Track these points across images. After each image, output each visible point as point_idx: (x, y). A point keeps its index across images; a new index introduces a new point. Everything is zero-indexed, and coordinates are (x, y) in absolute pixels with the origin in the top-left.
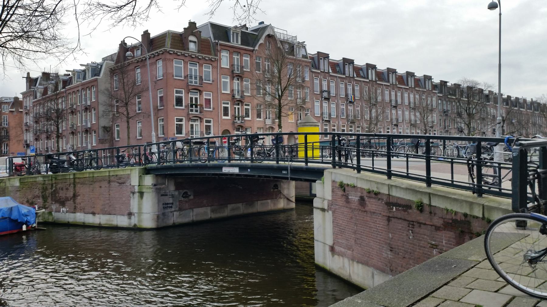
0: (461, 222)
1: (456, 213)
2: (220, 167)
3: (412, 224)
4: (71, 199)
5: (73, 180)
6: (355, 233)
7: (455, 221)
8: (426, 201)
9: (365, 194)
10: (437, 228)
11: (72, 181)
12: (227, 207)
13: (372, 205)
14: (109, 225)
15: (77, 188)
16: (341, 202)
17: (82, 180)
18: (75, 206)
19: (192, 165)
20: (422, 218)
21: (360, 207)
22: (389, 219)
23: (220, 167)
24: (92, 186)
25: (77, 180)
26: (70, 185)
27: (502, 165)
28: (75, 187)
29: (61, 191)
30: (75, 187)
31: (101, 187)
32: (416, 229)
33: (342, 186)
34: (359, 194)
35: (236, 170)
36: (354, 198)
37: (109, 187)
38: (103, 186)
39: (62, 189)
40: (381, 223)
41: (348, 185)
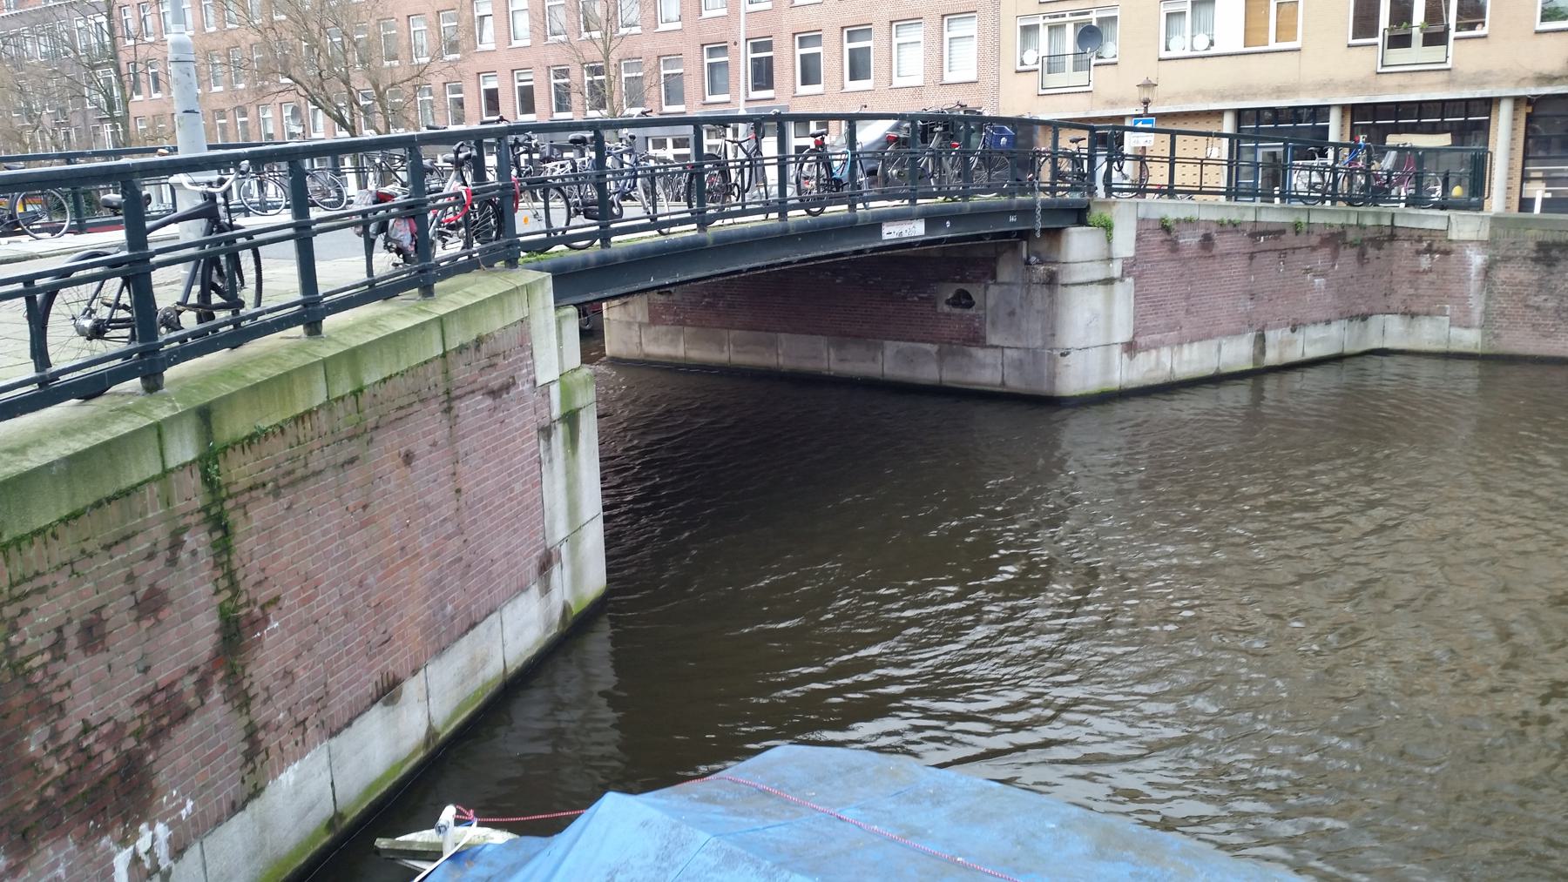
0: (1339, 234)
1: (1331, 226)
2: (875, 225)
3: (1283, 253)
4: (203, 686)
5: (194, 481)
6: (1188, 298)
7: (1333, 235)
8: (1304, 219)
9: (1214, 228)
10: (1314, 249)
11: (191, 494)
12: (881, 348)
13: (1223, 244)
14: (482, 689)
15: (246, 544)
16: (1160, 253)
17: (279, 449)
18: (251, 734)
19: (973, 208)
20: (1297, 242)
21: (1202, 253)
22: (1252, 256)
23: (875, 225)
24: (354, 475)
25: (239, 470)
26: (176, 544)
27: (257, 238)
28: (223, 547)
29: (80, 668)
30: (223, 547)
31: (408, 458)
32: (1289, 257)
33: (1165, 227)
34: (1202, 232)
35: (917, 229)
36: (1190, 240)
37: (452, 439)
38: (421, 447)
39: (93, 634)
40: (1239, 264)
41: (1178, 221)
